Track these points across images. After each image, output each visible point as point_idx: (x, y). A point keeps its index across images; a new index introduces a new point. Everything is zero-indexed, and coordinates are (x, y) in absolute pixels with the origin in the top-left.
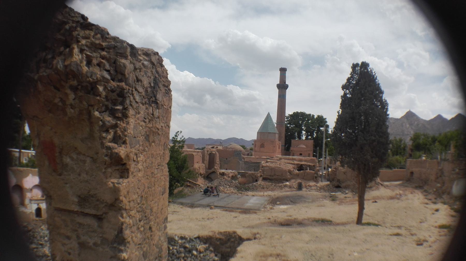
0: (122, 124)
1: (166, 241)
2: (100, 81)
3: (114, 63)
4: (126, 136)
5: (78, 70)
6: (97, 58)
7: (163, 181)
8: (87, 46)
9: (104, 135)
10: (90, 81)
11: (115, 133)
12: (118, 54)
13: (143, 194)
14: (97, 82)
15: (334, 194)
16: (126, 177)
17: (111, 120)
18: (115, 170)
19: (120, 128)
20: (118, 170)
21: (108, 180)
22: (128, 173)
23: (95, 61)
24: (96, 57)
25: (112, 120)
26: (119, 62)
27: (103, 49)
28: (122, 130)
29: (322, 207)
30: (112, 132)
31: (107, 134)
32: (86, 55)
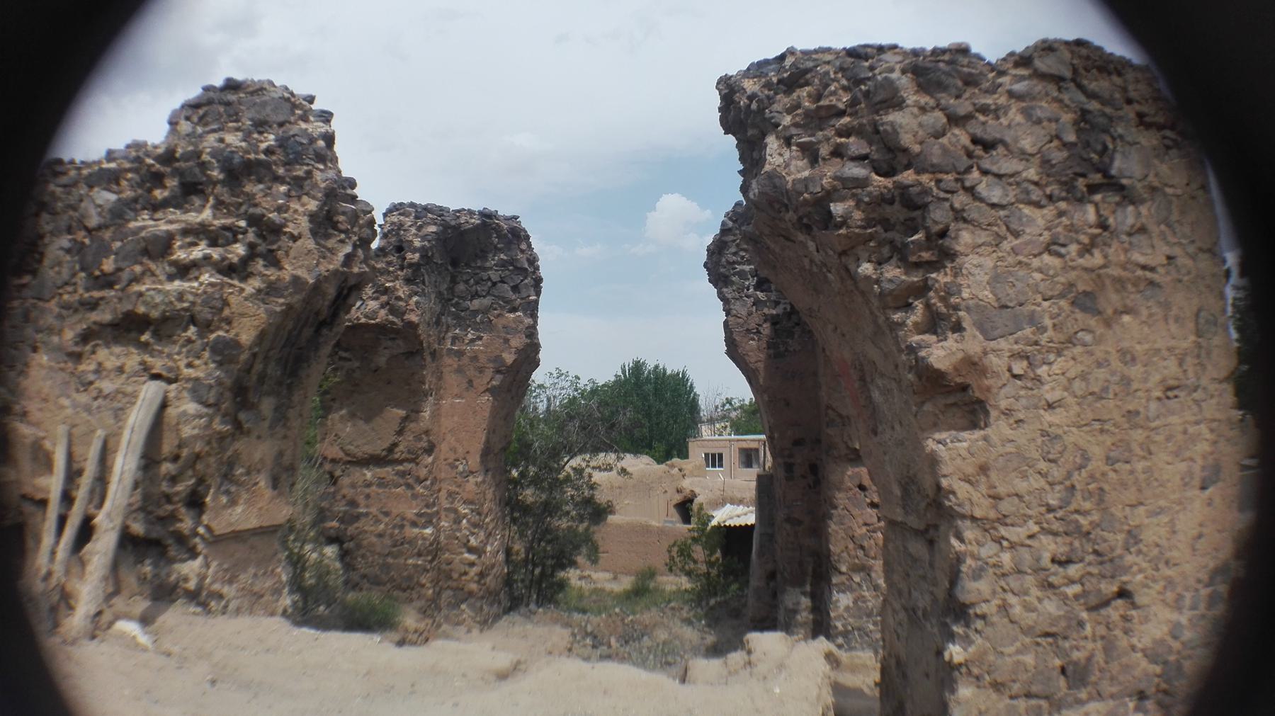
0: (941, 278)
1: (105, 554)
2: (835, 189)
3: (876, 134)
4: (956, 308)
5: (775, 187)
6: (828, 139)
7: (1207, 440)
8: (796, 125)
9: (897, 317)
10: (805, 200)
11: (928, 306)
12: (878, 106)
13: (1076, 475)
14: (829, 195)
15: (843, 140)
16: (982, 424)
17: (898, 275)
18: (947, 406)
19: (936, 291)
20: (954, 404)
21: (926, 435)
22: (987, 413)
23: (824, 151)
24: (826, 139)
25: (906, 274)
26: (882, 124)
27: (842, 113)
28: (942, 294)
29: (689, 673)
30: (919, 305)
31: (906, 312)
32: (798, 145)
